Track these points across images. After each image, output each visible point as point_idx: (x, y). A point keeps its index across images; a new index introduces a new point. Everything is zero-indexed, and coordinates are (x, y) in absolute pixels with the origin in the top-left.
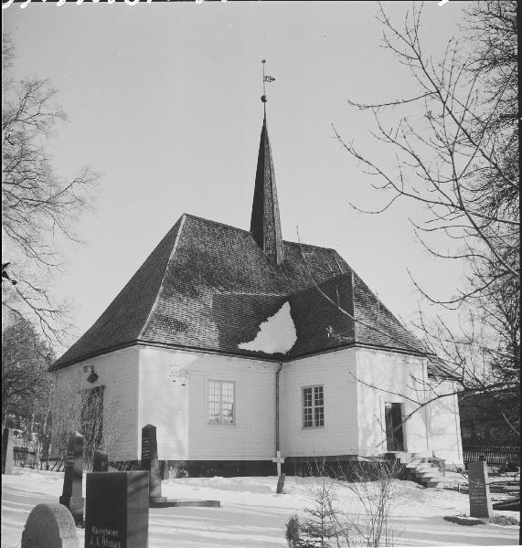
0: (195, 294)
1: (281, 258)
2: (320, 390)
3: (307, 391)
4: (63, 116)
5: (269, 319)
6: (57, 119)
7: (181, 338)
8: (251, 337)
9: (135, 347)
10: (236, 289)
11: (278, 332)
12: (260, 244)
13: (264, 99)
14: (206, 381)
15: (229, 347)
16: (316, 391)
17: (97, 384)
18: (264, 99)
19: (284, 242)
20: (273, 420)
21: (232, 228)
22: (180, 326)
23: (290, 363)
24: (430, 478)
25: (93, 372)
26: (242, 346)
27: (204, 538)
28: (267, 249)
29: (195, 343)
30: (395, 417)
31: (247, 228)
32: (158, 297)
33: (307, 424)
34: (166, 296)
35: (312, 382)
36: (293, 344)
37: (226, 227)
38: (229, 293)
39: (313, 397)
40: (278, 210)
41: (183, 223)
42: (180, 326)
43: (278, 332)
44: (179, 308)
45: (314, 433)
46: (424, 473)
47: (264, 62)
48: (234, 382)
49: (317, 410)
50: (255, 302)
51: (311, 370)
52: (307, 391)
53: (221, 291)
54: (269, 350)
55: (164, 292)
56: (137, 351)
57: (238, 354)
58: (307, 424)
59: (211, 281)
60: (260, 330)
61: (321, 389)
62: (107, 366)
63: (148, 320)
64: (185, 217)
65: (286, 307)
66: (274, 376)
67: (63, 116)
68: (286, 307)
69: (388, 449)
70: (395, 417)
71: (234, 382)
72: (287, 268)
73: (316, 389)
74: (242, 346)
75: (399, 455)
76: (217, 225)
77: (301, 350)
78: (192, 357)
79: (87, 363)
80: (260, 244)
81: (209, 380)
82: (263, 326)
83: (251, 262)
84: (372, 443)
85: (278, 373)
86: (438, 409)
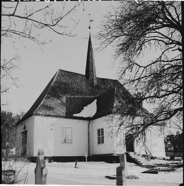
0: (59, 97)
1: (95, 82)
2: (102, 130)
3: (99, 130)
7: (51, 113)
8: (79, 112)
9: (33, 116)
10: (77, 95)
12: (88, 79)
13: (89, 28)
14: (61, 128)
15: (69, 115)
16: (101, 130)
17: (26, 130)
18: (89, 28)
19: (97, 78)
20: (88, 141)
21: (77, 74)
22: (50, 108)
23: (93, 121)
24: (140, 162)
25: (25, 126)
27: (165, 166)
28: (91, 81)
29: (56, 114)
31: (84, 74)
32: (44, 99)
33: (99, 143)
34: (47, 98)
35: (100, 127)
37: (75, 74)
38: (72, 96)
39: (101, 132)
40: (95, 66)
42: (50, 108)
43: (90, 110)
44: (53, 102)
45: (101, 145)
46: (138, 160)
47: (90, 15)
48: (72, 128)
49: (102, 137)
50: (83, 99)
51: (101, 123)
52: (99, 130)
53: (70, 96)
55: (47, 96)
56: (34, 118)
58: (99, 143)
59: (65, 93)
61: (103, 129)
63: (39, 106)
64: (59, 70)
65: (95, 101)
66: (87, 126)
68: (95, 101)
69: (127, 151)
71: (72, 128)
72: (98, 87)
73: (101, 129)
76: (71, 73)
78: (55, 119)
80: (88, 79)
81: (62, 127)
82: (85, 108)
83: (84, 86)
85: (89, 125)
86: (155, 137)
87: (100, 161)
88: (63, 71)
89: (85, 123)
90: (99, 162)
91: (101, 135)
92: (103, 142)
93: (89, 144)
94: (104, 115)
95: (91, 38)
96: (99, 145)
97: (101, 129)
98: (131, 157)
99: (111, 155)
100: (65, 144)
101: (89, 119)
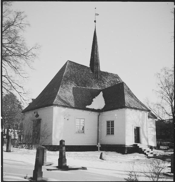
2: (113, 122)
3: (108, 122)
4: (29, 25)
5: (96, 97)
6: (27, 26)
11: (99, 102)
13: (95, 21)
18: (95, 21)
25: (37, 114)
26: (87, 107)
30: (137, 131)
35: (110, 119)
36: (104, 106)
41: (68, 63)
52: (108, 122)
54: (96, 108)
57: (86, 109)
60: (93, 101)
62: (43, 113)
65: (101, 93)
67: (29, 25)
68: (101, 93)
69: (135, 142)
70: (137, 131)
74: (87, 107)
75: (138, 145)
77: (105, 109)
78: (25, 161)
79: (36, 111)
81: (76, 118)
82: (94, 100)
84: (130, 142)
85: (99, 116)
87: (112, 151)
88: (72, 62)
89: (94, 115)
90: (109, 152)
91: (110, 126)
92: (113, 133)
93: (98, 134)
94: (116, 108)
95: (96, 32)
96: (108, 136)
97: (111, 122)
98: (93, 101)
99: (122, 146)
100: (98, 14)
101: (99, 111)
